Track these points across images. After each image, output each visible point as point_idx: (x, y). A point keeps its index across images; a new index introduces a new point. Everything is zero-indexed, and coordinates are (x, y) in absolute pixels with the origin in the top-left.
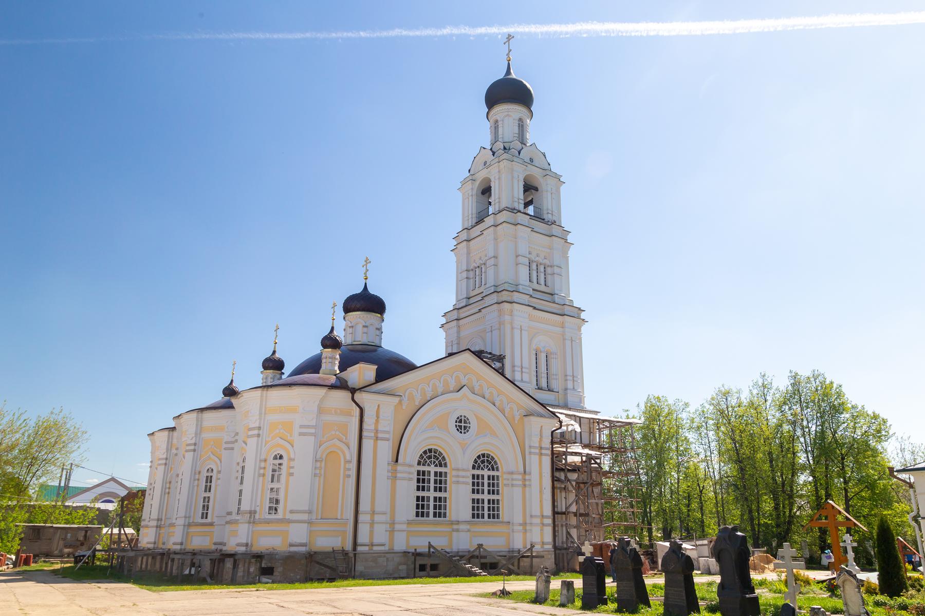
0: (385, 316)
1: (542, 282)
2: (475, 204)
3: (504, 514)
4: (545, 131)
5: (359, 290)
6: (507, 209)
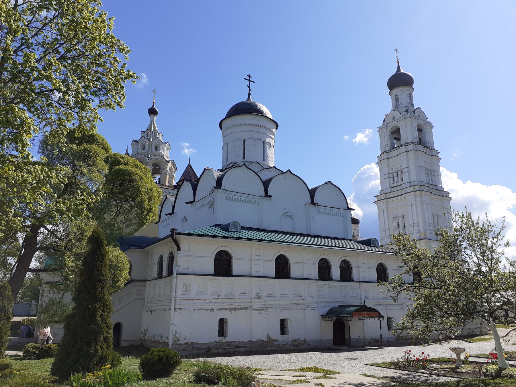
2: (389, 140)
4: (421, 97)
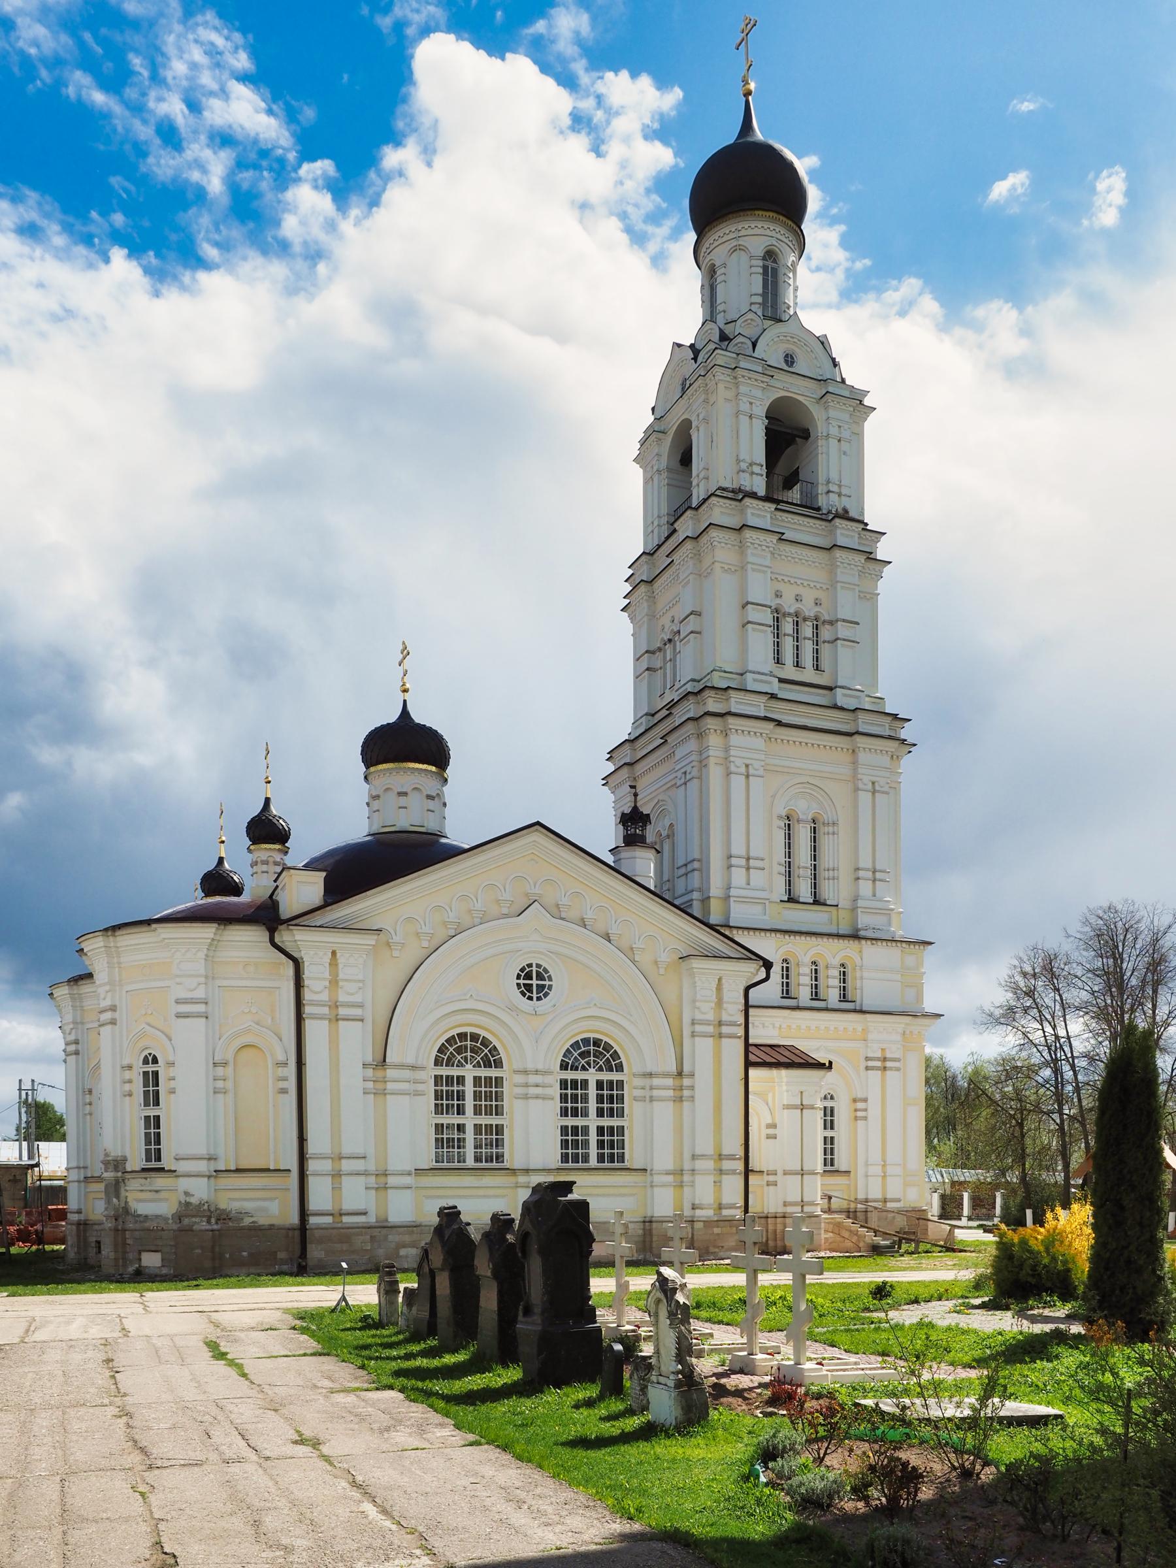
0: (450, 772)
1: (808, 659)
3: (634, 1154)
5: (392, 716)
6: (723, 493)
